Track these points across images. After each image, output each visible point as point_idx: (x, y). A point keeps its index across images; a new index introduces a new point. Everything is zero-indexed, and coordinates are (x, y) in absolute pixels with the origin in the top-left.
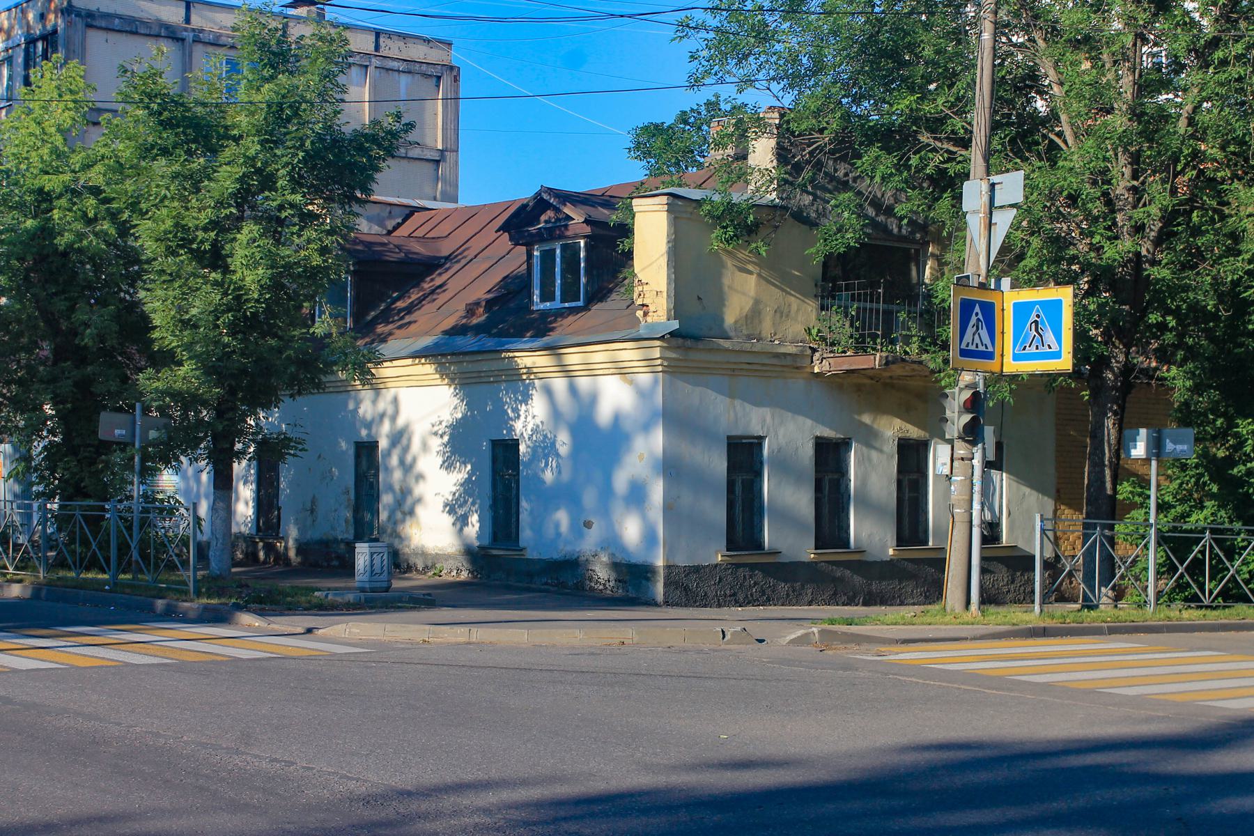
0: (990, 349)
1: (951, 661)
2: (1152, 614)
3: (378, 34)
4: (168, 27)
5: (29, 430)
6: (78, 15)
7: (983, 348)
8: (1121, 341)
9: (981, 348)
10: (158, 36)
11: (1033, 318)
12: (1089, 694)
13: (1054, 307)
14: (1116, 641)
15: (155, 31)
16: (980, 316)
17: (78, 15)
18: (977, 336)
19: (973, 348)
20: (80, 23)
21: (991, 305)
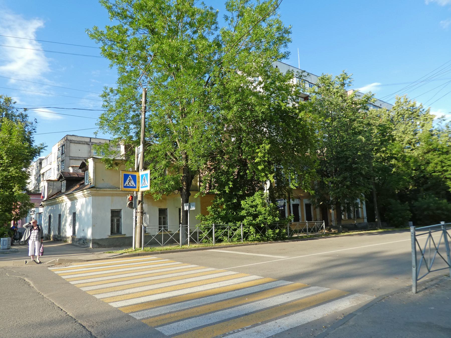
0: (135, 186)
1: (125, 267)
2: (142, 250)
3: (90, 138)
4: (86, 142)
5: (318, 197)
6: (68, 140)
7: (132, 186)
8: (18, 177)
9: (131, 185)
10: (84, 144)
11: (144, 178)
12: (184, 262)
13: (146, 175)
14: (153, 256)
15: (84, 143)
16: (131, 178)
17: (68, 140)
18: (130, 183)
19: (129, 185)
20: (69, 142)
21: (135, 176)
